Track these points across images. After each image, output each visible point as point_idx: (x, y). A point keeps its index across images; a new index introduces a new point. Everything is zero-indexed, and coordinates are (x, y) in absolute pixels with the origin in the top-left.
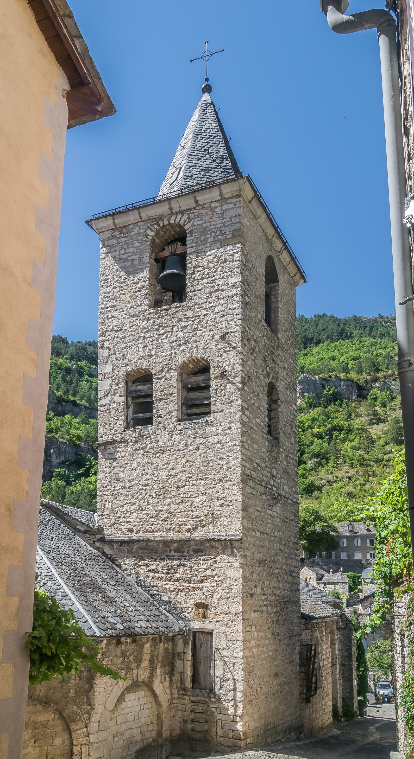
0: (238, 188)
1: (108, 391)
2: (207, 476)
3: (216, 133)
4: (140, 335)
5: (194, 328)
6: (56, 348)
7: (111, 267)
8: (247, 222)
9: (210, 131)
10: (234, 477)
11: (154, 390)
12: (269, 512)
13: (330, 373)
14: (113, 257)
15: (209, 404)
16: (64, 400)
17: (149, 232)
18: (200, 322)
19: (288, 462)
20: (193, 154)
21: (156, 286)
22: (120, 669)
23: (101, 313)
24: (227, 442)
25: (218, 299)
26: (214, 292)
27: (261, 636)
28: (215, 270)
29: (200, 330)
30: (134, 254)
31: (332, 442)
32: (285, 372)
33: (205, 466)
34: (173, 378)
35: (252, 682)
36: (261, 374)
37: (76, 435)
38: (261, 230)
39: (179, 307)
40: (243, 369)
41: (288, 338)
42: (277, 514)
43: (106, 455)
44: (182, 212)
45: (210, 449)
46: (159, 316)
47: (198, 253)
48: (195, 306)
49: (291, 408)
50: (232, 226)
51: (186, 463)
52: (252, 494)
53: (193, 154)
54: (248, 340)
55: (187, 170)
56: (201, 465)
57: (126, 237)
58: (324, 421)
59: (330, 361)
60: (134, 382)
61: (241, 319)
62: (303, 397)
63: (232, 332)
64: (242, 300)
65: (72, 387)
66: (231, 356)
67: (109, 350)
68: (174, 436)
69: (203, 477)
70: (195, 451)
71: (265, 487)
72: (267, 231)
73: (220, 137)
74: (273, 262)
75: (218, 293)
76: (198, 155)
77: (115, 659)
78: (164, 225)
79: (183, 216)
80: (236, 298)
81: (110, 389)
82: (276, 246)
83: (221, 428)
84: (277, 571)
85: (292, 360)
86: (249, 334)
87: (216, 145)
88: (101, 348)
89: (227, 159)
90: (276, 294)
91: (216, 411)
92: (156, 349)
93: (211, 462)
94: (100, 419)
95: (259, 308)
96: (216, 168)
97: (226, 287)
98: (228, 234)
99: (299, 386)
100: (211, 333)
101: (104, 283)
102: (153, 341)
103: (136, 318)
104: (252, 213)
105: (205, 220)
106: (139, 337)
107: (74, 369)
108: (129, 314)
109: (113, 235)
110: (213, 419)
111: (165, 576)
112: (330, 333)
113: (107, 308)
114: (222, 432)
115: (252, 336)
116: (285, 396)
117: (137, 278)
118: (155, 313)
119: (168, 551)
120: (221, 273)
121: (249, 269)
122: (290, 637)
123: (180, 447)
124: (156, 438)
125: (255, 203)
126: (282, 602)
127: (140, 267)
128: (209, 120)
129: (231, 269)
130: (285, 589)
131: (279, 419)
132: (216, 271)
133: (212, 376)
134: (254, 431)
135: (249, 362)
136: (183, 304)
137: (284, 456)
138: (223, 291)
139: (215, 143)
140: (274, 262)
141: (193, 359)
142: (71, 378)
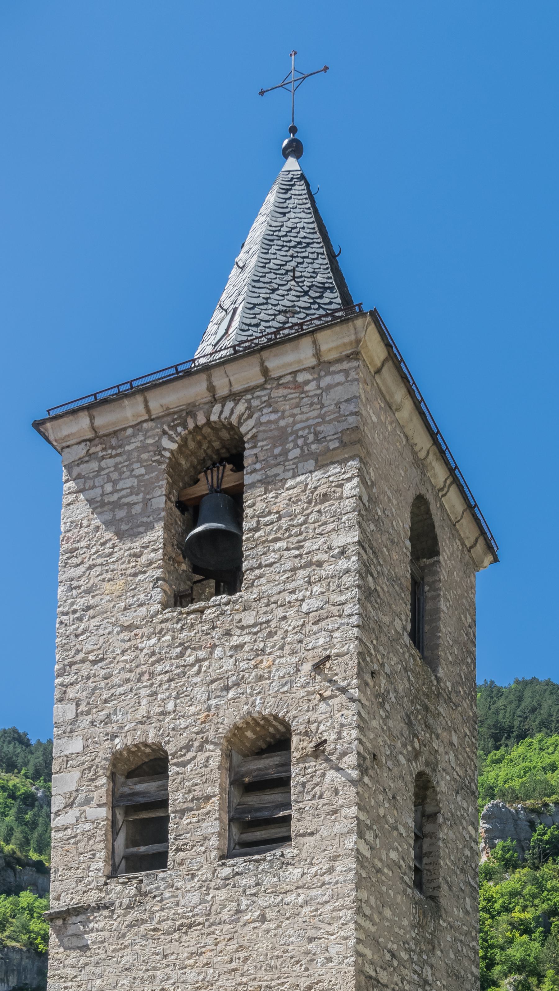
0: (353, 338)
1: (74, 794)
2: (282, 980)
3: (311, 236)
4: (144, 668)
5: (257, 650)
6: (7, 755)
7: (85, 523)
8: (372, 415)
9: (299, 232)
10: (339, 980)
11: (170, 789)
13: (546, 799)
14: (90, 501)
15: (287, 819)
16: (19, 861)
17: (166, 443)
18: (271, 635)
20: (261, 279)
21: (179, 563)
23: (61, 623)
24: (327, 902)
25: (309, 583)
26: (301, 567)
28: (303, 518)
29: (270, 654)
30: (133, 491)
31: (550, 939)
32: (452, 755)
33: (278, 957)
34: (211, 762)
36: (401, 753)
37: (42, 932)
38: (402, 435)
39: (227, 604)
40: (362, 737)
41: (458, 679)
43: (65, 940)
44: (235, 397)
45: (288, 919)
46: (183, 625)
47: (268, 483)
48: (259, 600)
49: (464, 833)
50: (339, 422)
51: (236, 951)
53: (261, 279)
54: (372, 673)
55: (248, 311)
56: (270, 956)
57: (117, 455)
58: (534, 896)
59: (546, 774)
60: (130, 775)
61: (358, 626)
62: (493, 847)
63: (338, 655)
64: (361, 582)
65: (36, 835)
66: (336, 708)
67: (78, 705)
68: (212, 892)
69: (274, 983)
70: (257, 924)
72: (416, 440)
73: (318, 246)
74: (428, 512)
75: (310, 569)
76: (271, 282)
78: (197, 426)
79: (236, 404)
80: (348, 580)
81: (77, 790)
82: (435, 476)
83: (313, 870)
85: (469, 728)
86: (375, 660)
87: (310, 261)
88: (61, 700)
89: (331, 289)
90: (434, 582)
91: (301, 832)
92: (176, 698)
93: (290, 948)
94: (55, 858)
95: (396, 606)
96: (309, 308)
97: (325, 557)
98: (331, 440)
99: (483, 826)
100: (295, 659)
101: (68, 558)
102: (170, 680)
103: (135, 632)
104: (383, 396)
105: (284, 412)
106: (142, 674)
107: (40, 798)
108: (120, 623)
109: (90, 452)
110: (295, 851)
112: (544, 717)
113: (75, 612)
114: (315, 880)
115: (382, 665)
116: (452, 806)
117: (137, 544)
118: (175, 621)
120: (317, 524)
121: (376, 517)
123: (225, 915)
124: (174, 897)
125: (388, 373)
127: (145, 520)
128: (297, 210)
129: (337, 517)
131: (439, 857)
132: (305, 522)
133: (295, 755)
134: (383, 878)
135: (375, 723)
136: (234, 597)
137: (449, 938)
138: (320, 564)
139: (308, 257)
140: (429, 510)
141: (254, 719)
142: (35, 815)
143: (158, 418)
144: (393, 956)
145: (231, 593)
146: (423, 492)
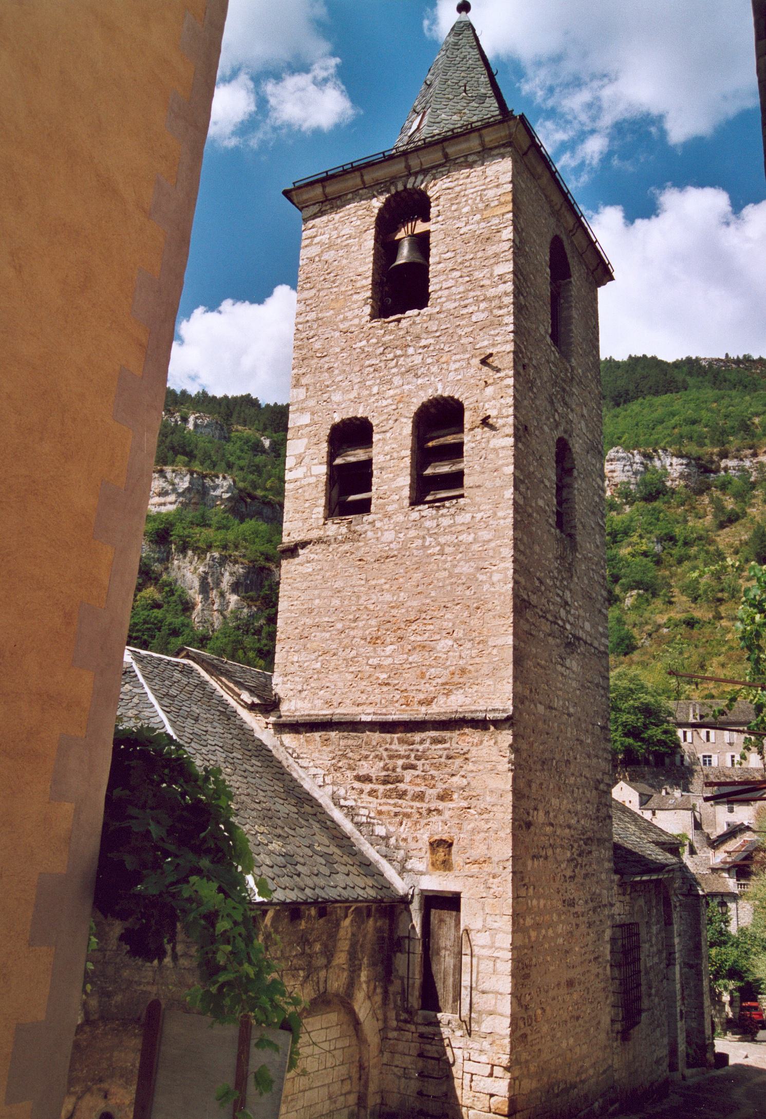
12: (559, 668)
16: (249, 495)
19: (590, 579)
22: (296, 969)
27: (545, 906)
35: (528, 997)
42: (573, 672)
52: (531, 634)
71: (551, 622)
77: (288, 949)
84: (572, 780)
111: (381, 788)
115: (531, 359)
116: (584, 463)
119: (389, 741)
122: (594, 910)
126: (581, 839)
130: (586, 815)
135: (526, 403)
136: (422, 311)
143: (371, 186)
144: (541, 582)
145: (421, 308)
146: (558, 233)
